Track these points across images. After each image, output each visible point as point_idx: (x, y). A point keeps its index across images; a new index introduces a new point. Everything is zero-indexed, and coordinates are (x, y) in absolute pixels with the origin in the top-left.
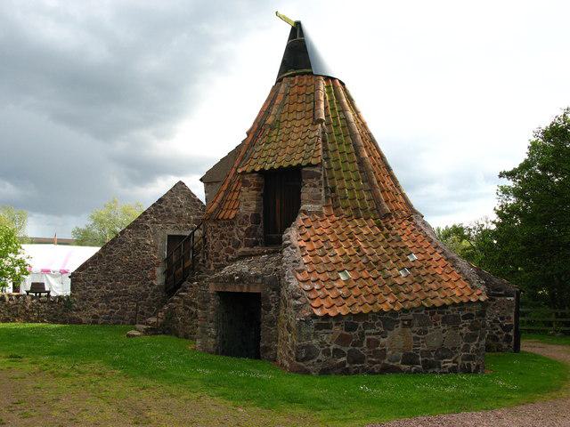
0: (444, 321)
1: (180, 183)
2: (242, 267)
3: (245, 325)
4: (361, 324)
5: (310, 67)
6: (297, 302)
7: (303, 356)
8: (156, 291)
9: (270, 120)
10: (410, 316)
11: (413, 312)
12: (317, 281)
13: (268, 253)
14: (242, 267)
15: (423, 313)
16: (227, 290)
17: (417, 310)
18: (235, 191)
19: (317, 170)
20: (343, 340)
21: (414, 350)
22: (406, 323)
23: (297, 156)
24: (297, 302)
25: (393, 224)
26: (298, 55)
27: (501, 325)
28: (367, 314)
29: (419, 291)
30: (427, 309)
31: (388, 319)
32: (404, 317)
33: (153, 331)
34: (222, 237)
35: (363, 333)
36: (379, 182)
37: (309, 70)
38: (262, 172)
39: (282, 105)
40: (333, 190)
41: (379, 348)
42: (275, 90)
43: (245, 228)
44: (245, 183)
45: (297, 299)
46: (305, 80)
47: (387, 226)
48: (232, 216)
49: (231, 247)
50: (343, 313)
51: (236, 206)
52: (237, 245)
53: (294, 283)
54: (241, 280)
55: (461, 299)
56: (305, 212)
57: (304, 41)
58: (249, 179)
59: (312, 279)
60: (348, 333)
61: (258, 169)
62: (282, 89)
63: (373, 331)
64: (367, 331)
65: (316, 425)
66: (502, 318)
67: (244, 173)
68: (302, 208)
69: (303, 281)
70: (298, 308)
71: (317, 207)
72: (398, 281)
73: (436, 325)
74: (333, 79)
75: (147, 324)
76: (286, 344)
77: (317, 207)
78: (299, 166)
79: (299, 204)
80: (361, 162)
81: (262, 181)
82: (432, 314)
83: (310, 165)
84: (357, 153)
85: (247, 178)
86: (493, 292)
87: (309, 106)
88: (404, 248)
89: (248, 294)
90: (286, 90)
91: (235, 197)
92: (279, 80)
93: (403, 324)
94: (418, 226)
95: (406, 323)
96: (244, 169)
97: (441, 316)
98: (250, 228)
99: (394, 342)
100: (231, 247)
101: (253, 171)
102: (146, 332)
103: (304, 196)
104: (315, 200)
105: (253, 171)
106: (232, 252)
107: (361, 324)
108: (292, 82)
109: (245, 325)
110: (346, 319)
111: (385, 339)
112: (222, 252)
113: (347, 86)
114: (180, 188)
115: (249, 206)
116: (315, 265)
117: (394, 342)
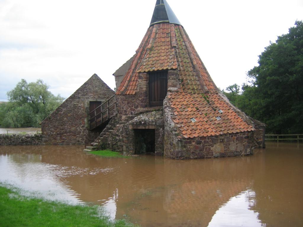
0: (237, 139)
1: (95, 74)
2: (143, 117)
3: (147, 142)
4: (203, 141)
5: (168, 19)
6: (176, 133)
7: (180, 155)
8: (85, 130)
9: (149, 46)
10: (222, 138)
11: (224, 136)
12: (182, 123)
13: (155, 110)
14: (143, 117)
15: (228, 136)
16: (139, 128)
17: (225, 135)
18: (134, 81)
19: (176, 72)
20: (196, 148)
21: (225, 152)
22: (221, 140)
23: (166, 65)
24: (176, 133)
25: (209, 96)
26: (161, 15)
27: (257, 142)
28: (205, 137)
29: (226, 126)
30: (230, 134)
31: (214, 139)
32: (220, 138)
33: (97, 149)
34: (128, 103)
35: (204, 145)
36: (202, 76)
37: (167, 21)
38: (149, 72)
39: (155, 38)
40: (182, 81)
41: (210, 151)
42: (150, 31)
43: (140, 99)
44: (140, 77)
45: (175, 131)
46: (166, 26)
47: (208, 98)
48: (134, 93)
49: (133, 108)
50: (196, 136)
51: (136, 88)
52: (137, 107)
53: (173, 124)
54: (145, 123)
55: (216, 133)
56: (170, 91)
57: (164, 6)
58: (142, 75)
59: (180, 122)
60: (198, 145)
61: (147, 71)
62: (154, 29)
63: (208, 144)
64: (206, 144)
65: (38, 226)
66: (257, 139)
67: (140, 73)
68: (169, 89)
69: (177, 123)
70: (176, 135)
71: (175, 89)
72: (216, 122)
73: (233, 141)
74: (178, 25)
75: (92, 145)
76: (168, 150)
77: (175, 89)
78: (167, 70)
79: (166, 87)
80: (194, 67)
81: (148, 76)
82: (232, 136)
83: (172, 69)
84: (192, 63)
85: (141, 75)
86: (257, 126)
87: (168, 39)
88: (216, 107)
89: (148, 130)
90: (156, 31)
91: (134, 84)
92: (152, 25)
93: (220, 141)
94: (221, 97)
95: (221, 140)
96: (139, 71)
97: (236, 137)
98: (143, 99)
99: (217, 148)
100: (133, 108)
101: (145, 72)
102: (93, 149)
103: (169, 83)
104: (174, 86)
105: (145, 72)
106: (134, 110)
107: (203, 141)
108: (159, 27)
109: (147, 142)
110: (197, 139)
111: (213, 148)
112: (128, 110)
113: (184, 28)
114: (95, 79)
115: (142, 88)
116: (180, 116)
117: (217, 148)
